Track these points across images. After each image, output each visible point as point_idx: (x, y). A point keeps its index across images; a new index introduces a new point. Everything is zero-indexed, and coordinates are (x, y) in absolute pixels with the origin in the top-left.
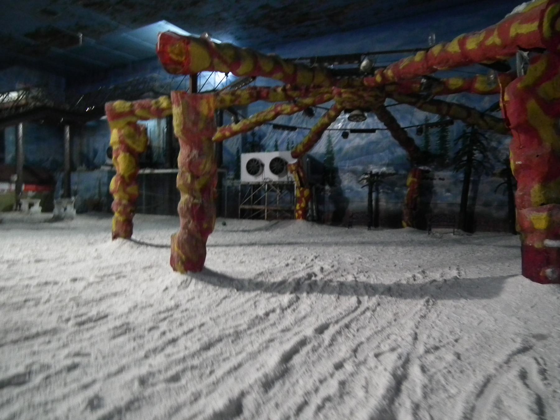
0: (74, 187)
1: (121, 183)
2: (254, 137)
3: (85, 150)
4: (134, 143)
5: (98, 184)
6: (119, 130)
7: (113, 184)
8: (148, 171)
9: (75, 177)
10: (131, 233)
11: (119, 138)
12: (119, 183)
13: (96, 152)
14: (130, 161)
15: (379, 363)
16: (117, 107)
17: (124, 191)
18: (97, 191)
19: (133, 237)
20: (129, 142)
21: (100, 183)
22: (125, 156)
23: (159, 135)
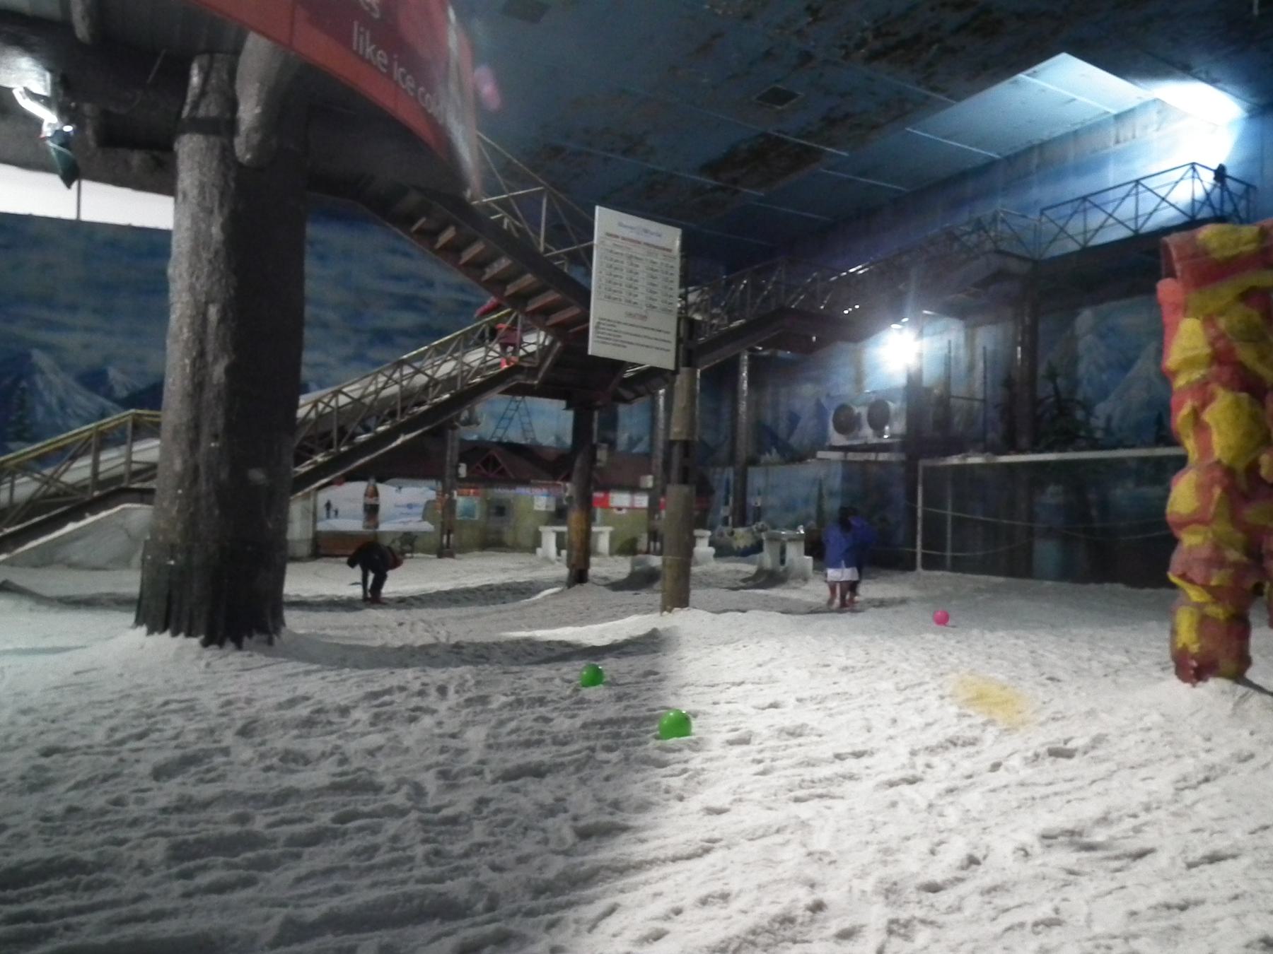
0: (755, 501)
1: (1226, 490)
2: (1054, 382)
3: (768, 418)
4: (1262, 358)
5: (815, 490)
6: (1209, 320)
7: (1183, 496)
8: (955, 460)
9: (756, 478)
10: (1244, 661)
11: (1212, 344)
12: (1217, 491)
13: (794, 419)
14: (1169, 420)
15: (1052, 885)
16: (1214, 244)
17: (1235, 519)
18: (812, 510)
19: (1252, 674)
20: (1246, 355)
21: (820, 490)
22: (1237, 404)
23: (971, 368)
